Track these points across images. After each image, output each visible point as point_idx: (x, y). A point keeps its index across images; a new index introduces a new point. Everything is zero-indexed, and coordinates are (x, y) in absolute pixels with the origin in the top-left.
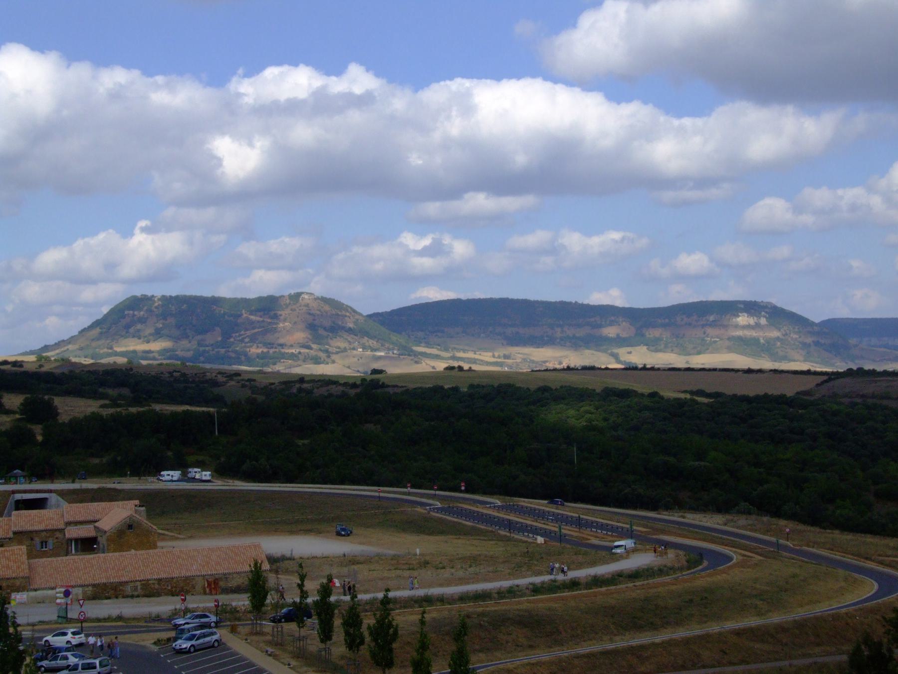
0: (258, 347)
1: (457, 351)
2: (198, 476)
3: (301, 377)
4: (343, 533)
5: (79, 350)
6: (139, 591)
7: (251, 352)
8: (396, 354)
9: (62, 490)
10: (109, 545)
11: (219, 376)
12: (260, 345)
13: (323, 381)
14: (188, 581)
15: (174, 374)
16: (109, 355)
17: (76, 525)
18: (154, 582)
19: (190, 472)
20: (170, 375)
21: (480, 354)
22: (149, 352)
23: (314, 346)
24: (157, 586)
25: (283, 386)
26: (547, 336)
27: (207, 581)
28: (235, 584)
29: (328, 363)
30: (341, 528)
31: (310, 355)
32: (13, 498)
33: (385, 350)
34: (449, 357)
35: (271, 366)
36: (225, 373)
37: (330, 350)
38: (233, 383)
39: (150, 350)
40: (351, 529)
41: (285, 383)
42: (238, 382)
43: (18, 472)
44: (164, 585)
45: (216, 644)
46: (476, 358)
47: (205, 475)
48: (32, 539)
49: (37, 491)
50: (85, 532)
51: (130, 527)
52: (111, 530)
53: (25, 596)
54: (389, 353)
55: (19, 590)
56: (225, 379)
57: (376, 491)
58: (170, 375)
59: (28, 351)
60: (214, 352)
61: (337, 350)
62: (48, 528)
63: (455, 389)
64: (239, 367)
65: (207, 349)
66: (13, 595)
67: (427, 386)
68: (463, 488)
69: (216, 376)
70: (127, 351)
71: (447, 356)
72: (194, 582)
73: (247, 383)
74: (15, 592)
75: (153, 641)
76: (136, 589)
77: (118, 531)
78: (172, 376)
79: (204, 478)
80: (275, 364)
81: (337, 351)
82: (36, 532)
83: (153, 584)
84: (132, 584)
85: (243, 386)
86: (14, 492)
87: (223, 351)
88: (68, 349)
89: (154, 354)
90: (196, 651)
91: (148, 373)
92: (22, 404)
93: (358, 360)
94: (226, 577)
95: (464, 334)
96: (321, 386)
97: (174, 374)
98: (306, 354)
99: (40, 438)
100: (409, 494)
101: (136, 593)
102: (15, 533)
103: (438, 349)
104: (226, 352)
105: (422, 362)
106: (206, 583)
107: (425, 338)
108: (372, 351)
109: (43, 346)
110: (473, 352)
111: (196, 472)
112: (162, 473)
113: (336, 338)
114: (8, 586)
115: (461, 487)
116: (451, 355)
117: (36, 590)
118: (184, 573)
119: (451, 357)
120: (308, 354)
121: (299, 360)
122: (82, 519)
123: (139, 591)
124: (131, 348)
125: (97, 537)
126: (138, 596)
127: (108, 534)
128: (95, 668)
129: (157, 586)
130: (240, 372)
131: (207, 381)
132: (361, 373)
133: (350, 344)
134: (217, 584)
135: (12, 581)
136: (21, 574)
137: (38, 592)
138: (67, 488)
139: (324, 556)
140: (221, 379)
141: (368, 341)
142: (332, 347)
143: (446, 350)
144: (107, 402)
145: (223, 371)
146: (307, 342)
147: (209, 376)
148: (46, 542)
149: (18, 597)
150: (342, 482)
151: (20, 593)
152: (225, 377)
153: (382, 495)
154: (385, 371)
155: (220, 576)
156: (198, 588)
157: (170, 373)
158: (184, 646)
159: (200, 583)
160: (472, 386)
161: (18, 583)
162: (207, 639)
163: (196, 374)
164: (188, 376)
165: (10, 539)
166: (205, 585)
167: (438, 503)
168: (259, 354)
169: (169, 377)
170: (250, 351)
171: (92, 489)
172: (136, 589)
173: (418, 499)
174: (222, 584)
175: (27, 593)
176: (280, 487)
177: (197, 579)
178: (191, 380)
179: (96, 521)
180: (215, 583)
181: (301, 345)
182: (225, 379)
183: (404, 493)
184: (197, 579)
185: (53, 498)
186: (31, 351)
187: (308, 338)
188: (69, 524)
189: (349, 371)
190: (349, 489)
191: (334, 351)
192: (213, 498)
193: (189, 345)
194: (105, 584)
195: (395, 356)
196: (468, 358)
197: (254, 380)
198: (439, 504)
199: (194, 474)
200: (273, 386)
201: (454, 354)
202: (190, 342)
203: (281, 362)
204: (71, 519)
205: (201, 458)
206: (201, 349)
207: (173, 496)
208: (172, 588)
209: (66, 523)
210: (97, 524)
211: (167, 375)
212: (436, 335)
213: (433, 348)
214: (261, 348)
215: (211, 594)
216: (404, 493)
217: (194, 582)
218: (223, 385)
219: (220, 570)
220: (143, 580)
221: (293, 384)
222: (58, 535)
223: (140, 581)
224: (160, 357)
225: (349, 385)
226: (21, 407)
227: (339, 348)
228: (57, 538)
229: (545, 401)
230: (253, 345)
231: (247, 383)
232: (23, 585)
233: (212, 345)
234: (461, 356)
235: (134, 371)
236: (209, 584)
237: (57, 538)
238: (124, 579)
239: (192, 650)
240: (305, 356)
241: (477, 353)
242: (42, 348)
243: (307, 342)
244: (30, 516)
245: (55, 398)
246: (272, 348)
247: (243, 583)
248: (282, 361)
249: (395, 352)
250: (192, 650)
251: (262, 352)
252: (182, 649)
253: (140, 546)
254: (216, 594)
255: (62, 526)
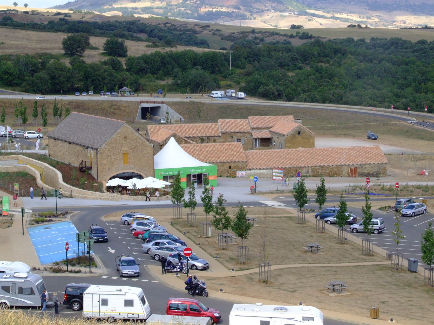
0: (206, 7)
1: (335, 13)
2: (234, 95)
3: (253, 29)
4: (373, 137)
5: (91, 6)
6: (310, 173)
7: (201, 11)
8: (296, 14)
9: (169, 102)
10: (286, 144)
11: (196, 27)
12: (207, 6)
13: (268, 32)
14: (339, 168)
15: (167, 25)
16: (110, 10)
17: (258, 130)
18: (319, 168)
19: (228, 92)
20: (164, 25)
21: (351, 16)
22: (136, 8)
23: (242, 8)
24: (320, 171)
25: (241, 35)
26: (396, 4)
27: (350, 168)
28: (367, 171)
29: (251, 19)
30: (371, 135)
31: (240, 13)
32: (141, 106)
33: (288, 11)
34: (330, 17)
35: (214, 20)
36: (200, 25)
37: (252, 11)
38: (205, 32)
39: (136, 7)
40: (377, 135)
41: (242, 33)
42: (210, 31)
43: (125, 89)
44: (325, 170)
45: (425, 212)
46: (348, 18)
47: (241, 95)
48: (232, 138)
49: (155, 102)
50: (265, 134)
51: (299, 133)
52: (288, 134)
53: (244, 173)
54: (291, 14)
55: (241, 169)
56: (200, 29)
57: (372, 110)
58: (164, 25)
59: (58, 5)
60: (177, 10)
61: (258, 11)
62: (242, 131)
63: (363, 41)
64: (210, 22)
65: (173, 7)
66: (238, 172)
67: (342, 38)
68: (426, 110)
69: (194, 27)
70: (121, 8)
71: (329, 17)
72: (342, 169)
73: (216, 32)
74: (239, 170)
75: (380, 207)
76: (308, 171)
77: (291, 135)
78: (166, 26)
79: (240, 96)
80: (216, 19)
81: (257, 11)
82: (235, 133)
83: (319, 169)
84: (306, 169)
85: (214, 34)
86: (141, 102)
87: (183, 9)
88: (83, 5)
89: (139, 10)
90: (415, 216)
91: (150, 23)
92: (105, 44)
93: (271, 18)
94: (361, 166)
95: (340, 2)
96: (268, 36)
97: (167, 25)
98: (237, 13)
99: (125, 67)
100: (392, 112)
101: (308, 174)
102: (222, 133)
103: (323, 12)
104: (185, 10)
105: (313, 20)
106: (350, 170)
107: (314, 4)
108: (280, 12)
109: (67, 2)
110: (346, 14)
111: (232, 92)
112: (213, 92)
113: (257, 3)
114: (235, 167)
115: (424, 109)
116: (332, 15)
117: (250, 170)
118: (336, 163)
119: (332, 17)
120: (238, 13)
121: (233, 16)
122: (261, 126)
123: (310, 173)
124: (124, 6)
125: (272, 138)
126: (310, 176)
127: (286, 137)
128: (377, 224)
129: (320, 171)
130: (210, 25)
131: (189, 30)
132: (273, 26)
133: (266, 7)
134: (356, 171)
135: (237, 164)
136: (242, 160)
137: (252, 171)
138: (172, 101)
139: (390, 153)
140: (198, 29)
141: (277, 5)
142: (254, 8)
143: (328, 12)
144: (150, 44)
145: (198, 24)
146: (238, 5)
147: (189, 27)
148: (240, 140)
149: (240, 173)
150: (324, 102)
151: (242, 171)
152: (200, 28)
153: (376, 112)
154: (302, 26)
155: (358, 166)
156: (345, 172)
157: (164, 24)
158: (409, 213)
159: (346, 170)
160: (373, 39)
161: (240, 165)
162: (421, 209)
163: (181, 25)
164: (176, 26)
165: (219, 137)
166: (349, 171)
167: (415, 119)
168: (206, 11)
169: (163, 27)
170: (200, 10)
171: (187, 102)
172: (308, 171)
173: (400, 116)
174: (359, 171)
175: (245, 171)
176: (304, 105)
177: (344, 167)
178: (178, 29)
179: (270, 128)
180: (355, 170)
181: (234, 7)
182: (200, 29)
183: (389, 112)
184: (344, 167)
185: (164, 108)
186: (59, 5)
187: (239, 2)
188: (254, 129)
189: (265, 25)
190: (333, 107)
191: (255, 12)
192: (264, 110)
193: (162, 4)
194: (290, 168)
195: (295, 15)
196: (343, 18)
197: (220, 30)
198: (416, 120)
199: (231, 93)
200: (234, 35)
201: (334, 15)
202: (162, 3)
203: (221, 18)
204: (255, 126)
205: (228, 83)
206: (169, 8)
207: (238, 109)
208: (329, 172)
209: (253, 128)
210: (271, 130)
211: (162, 25)
212: (321, 2)
213: (320, 11)
214: (208, 8)
215: (352, 176)
216: (389, 112)
217: (342, 169)
218: (200, 33)
219: (358, 162)
220: (313, 167)
221: (248, 34)
222: (247, 135)
223: (311, 167)
224: (142, 12)
225: (288, 36)
226: (105, 46)
227: (258, 9)
228: (247, 137)
229: (425, 50)
230: (203, 6)
231: (216, 32)
232: (243, 166)
233: (176, 5)
234: (338, 17)
235: (141, 22)
236: (351, 171)
237: (247, 137)
238: (301, 165)
239: (413, 215)
240: (236, 14)
241: (349, 14)
242: (67, 4)
243: (238, 5)
244: (229, 123)
245: (125, 40)
246: (215, 8)
247: (371, 171)
248: (221, 17)
249: (295, 13)
250: (413, 215)
251: (209, 10)
252: (407, 214)
253: (304, 145)
254: (356, 177)
255: (249, 130)
